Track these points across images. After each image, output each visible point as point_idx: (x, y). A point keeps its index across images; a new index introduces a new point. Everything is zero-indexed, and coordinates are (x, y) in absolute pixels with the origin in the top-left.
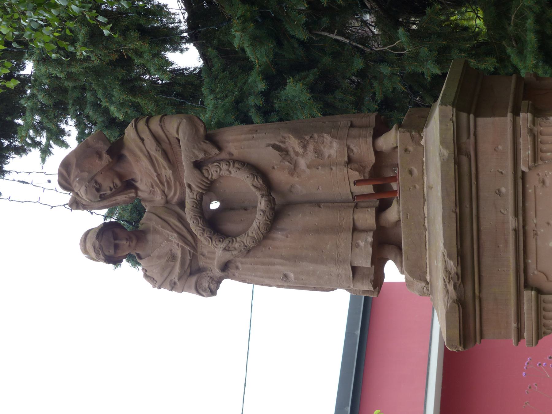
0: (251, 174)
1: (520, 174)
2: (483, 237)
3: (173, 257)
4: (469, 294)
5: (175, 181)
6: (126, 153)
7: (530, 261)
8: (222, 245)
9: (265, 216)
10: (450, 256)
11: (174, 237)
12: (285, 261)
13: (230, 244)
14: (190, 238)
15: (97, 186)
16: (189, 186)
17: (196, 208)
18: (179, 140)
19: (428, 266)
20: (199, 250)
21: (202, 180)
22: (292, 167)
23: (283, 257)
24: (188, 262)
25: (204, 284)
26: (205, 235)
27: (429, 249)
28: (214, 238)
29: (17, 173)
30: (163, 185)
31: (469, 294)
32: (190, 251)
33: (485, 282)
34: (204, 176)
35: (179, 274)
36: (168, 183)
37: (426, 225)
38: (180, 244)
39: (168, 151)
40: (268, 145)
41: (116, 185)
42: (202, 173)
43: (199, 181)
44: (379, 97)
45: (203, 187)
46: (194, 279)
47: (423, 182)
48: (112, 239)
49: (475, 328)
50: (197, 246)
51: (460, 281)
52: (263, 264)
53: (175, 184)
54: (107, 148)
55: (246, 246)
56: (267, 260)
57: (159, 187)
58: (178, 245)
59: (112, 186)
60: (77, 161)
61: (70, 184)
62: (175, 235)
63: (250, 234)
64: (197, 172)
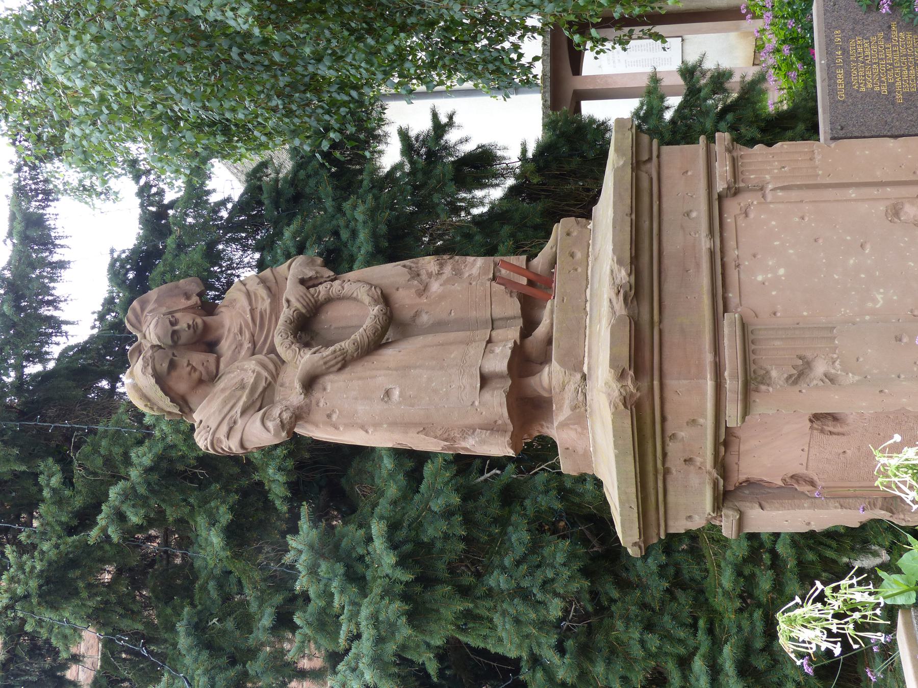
1: (716, 196)
2: (666, 262)
4: (645, 317)
7: (730, 295)
10: (620, 262)
16: (288, 301)
19: (586, 354)
20: (279, 380)
22: (421, 287)
24: (260, 389)
27: (590, 327)
31: (645, 317)
32: (266, 379)
33: (667, 312)
35: (245, 403)
37: (588, 309)
44: (530, 512)
47: (588, 265)
49: (653, 363)
51: (633, 292)
52: (359, 378)
57: (249, 328)
58: (253, 372)
61: (140, 322)
64: (302, 288)
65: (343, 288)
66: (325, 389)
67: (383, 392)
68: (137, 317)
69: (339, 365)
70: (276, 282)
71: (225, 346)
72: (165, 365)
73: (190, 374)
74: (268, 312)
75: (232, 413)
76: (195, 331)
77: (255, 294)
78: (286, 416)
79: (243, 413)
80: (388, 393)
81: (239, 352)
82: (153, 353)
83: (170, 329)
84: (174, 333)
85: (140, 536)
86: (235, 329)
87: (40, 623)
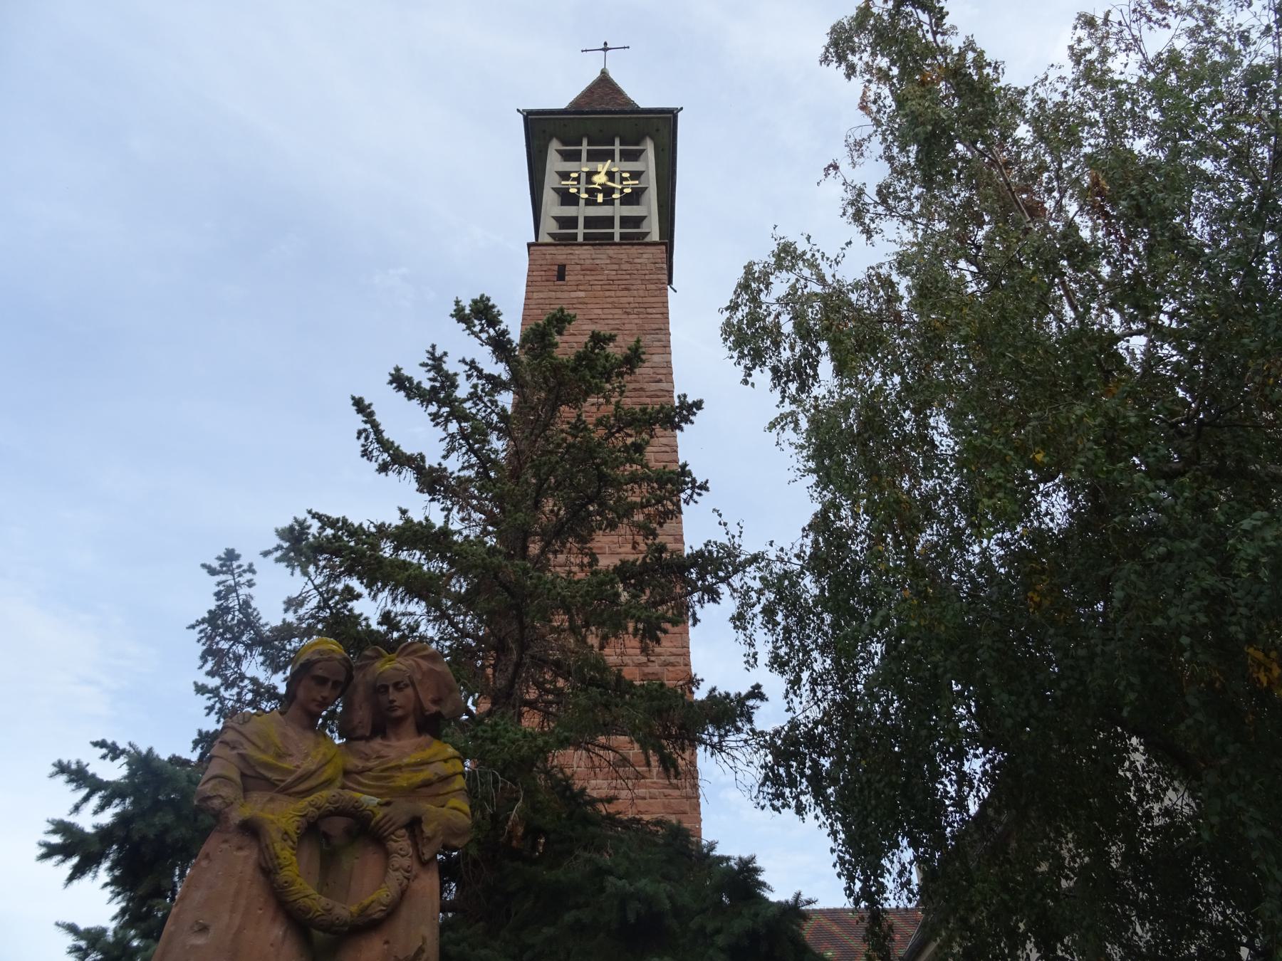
3: (280, 756)
5: (388, 788)
6: (426, 738)
8: (292, 829)
11: (309, 765)
14: (302, 787)
15: (402, 685)
16: (388, 804)
20: (280, 796)
28: (303, 820)
29: (778, 444)
30: (383, 771)
36: (385, 778)
39: (433, 787)
40: (424, 939)
42: (401, 828)
46: (235, 776)
53: (381, 787)
54: (444, 712)
57: (382, 763)
58: (298, 767)
61: (408, 655)
62: (313, 767)
63: (300, 880)
64: (404, 819)
65: (397, 870)
66: (240, 848)
68: (415, 652)
70: (439, 795)
71: (377, 744)
72: (320, 673)
73: (314, 700)
75: (247, 744)
78: (216, 803)
79: (242, 757)
80: (204, 929)
85: (1139, 758)
86: (384, 752)
87: (610, 175)
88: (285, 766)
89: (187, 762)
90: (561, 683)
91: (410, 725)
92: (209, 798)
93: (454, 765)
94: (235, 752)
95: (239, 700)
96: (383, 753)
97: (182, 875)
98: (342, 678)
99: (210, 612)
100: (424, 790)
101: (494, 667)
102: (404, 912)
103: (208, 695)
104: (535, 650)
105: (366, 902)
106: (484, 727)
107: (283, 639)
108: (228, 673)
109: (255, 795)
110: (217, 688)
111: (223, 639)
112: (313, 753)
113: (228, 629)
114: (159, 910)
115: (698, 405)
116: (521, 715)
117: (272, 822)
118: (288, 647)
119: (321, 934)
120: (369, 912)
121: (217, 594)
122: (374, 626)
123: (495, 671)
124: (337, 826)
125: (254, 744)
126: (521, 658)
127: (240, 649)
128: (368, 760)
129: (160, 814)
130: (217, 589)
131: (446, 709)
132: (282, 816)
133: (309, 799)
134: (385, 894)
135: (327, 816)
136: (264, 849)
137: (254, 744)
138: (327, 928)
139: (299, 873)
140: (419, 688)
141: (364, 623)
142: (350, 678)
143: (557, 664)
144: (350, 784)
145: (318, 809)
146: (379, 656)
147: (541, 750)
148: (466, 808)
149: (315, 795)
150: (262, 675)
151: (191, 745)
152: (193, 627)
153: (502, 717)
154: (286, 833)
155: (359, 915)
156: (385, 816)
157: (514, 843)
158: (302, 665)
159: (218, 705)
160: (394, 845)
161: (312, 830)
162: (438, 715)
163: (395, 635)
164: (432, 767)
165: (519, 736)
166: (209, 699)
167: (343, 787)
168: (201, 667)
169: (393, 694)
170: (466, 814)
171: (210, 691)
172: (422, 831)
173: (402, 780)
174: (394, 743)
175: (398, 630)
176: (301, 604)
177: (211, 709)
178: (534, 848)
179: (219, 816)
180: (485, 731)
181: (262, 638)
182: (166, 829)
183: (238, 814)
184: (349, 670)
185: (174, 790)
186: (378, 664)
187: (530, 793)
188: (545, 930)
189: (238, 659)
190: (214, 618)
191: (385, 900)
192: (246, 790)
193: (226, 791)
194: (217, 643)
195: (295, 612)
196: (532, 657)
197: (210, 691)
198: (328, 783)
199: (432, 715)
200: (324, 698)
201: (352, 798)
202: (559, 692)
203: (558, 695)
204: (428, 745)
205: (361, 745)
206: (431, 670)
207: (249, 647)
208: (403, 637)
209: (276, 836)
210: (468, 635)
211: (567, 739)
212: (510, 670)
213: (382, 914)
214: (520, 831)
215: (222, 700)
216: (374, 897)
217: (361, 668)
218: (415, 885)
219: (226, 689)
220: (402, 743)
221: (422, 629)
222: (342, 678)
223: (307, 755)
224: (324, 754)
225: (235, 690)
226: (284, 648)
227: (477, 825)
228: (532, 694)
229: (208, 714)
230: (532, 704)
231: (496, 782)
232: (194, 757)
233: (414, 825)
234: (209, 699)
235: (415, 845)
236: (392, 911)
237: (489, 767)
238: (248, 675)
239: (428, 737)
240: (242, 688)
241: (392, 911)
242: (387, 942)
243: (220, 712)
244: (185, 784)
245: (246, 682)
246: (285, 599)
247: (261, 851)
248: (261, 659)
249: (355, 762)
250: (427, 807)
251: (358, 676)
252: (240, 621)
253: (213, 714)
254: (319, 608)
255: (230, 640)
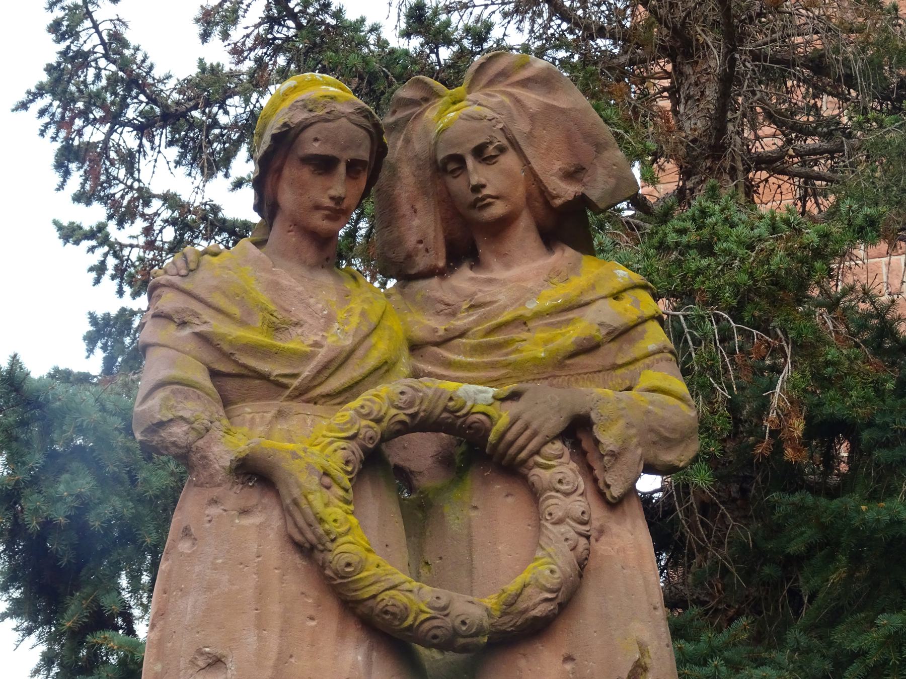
0: (561, 584)
3: (276, 329)
5: (507, 365)
6: (565, 255)
8: (335, 465)
9: (433, 613)
11: (338, 338)
12: (271, 663)
13: (341, 493)
15: (491, 151)
16: (515, 396)
17: (446, 409)
18: (629, 389)
20: (296, 406)
21: (535, 434)
23: (283, 658)
24: (264, 367)
25: (190, 405)
26: (364, 422)
28: (353, 445)
32: (295, 376)
34: (545, 443)
35: (223, 337)
36: (498, 346)
38: (322, 351)
40: (643, 648)
41: (490, 204)
43: (534, 425)
45: (509, 436)
48: (351, 154)
50: (308, 401)
52: (261, 592)
53: (493, 366)
54: (594, 194)
55: (333, 541)
56: (275, 608)
57: (477, 323)
58: (316, 344)
59: (486, 192)
60: (562, 111)
61: (491, 83)
62: (348, 342)
63: (373, 558)
64: (555, 422)
66: (245, 512)
67: (219, 651)
68: (504, 74)
69: (298, 537)
70: (615, 367)
71: (464, 279)
72: (315, 148)
73: (318, 207)
74: (513, 357)
75: (206, 314)
76: (473, 205)
77: (569, 322)
78: (178, 432)
79: (204, 338)
81: (438, 313)
82: (342, 115)
83: (465, 150)
84: (459, 160)
88: (291, 345)
89: (84, 378)
90: (828, 106)
91: (524, 232)
92: (161, 424)
93: (636, 303)
94: (187, 331)
95: (150, 245)
96: (480, 297)
97: (136, 587)
98: (364, 154)
99: (50, 69)
100: (582, 360)
101: (673, 93)
102: (591, 600)
103: (86, 244)
104: (759, 38)
105: (512, 587)
106: (679, 224)
107: (208, 103)
108: (117, 190)
109: (246, 410)
110: (101, 227)
111: (87, 122)
112: (341, 315)
113: (94, 100)
114: (110, 651)
115: (88, 252)
116: (750, 190)
117: (295, 455)
118: (223, 119)
119: (435, 654)
120: (521, 605)
121: (55, 27)
122: (396, 42)
123: (676, 103)
124: (420, 452)
125: (219, 310)
126: (732, 62)
127: (128, 139)
128: (453, 314)
129: (65, 477)
130: (50, 18)
131: (597, 189)
132: (312, 443)
133: (356, 403)
134: (547, 568)
135: (399, 433)
136: (290, 509)
137: (219, 310)
138: (446, 643)
139: (368, 540)
140: (529, 152)
141: (372, 39)
142: (380, 150)
143: (818, 65)
144: (429, 368)
145: (378, 421)
146: (430, 96)
147: (818, 253)
148: (679, 385)
149: (365, 395)
150: (185, 184)
151: (84, 346)
152: (24, 106)
153: (713, 194)
154: (326, 474)
155: (504, 614)
156: (513, 423)
157: (789, 453)
158: (274, 137)
159: (111, 262)
160: (545, 474)
161: (374, 463)
162: (582, 203)
163: (445, 53)
164: (590, 313)
165: (762, 229)
166: (92, 249)
167: (416, 374)
168: (61, 187)
169: (477, 173)
170: (681, 399)
171: (90, 235)
172: (597, 442)
173: (536, 345)
174: (499, 272)
175: (448, 42)
176: (232, 18)
177: (100, 269)
178: (830, 459)
179: (187, 459)
180: (682, 232)
181: (164, 107)
182: (84, 506)
183: (226, 447)
184: (376, 134)
185: (80, 430)
186: (430, 114)
187: (806, 349)
188: (882, 620)
189: (129, 160)
190: (60, 80)
191: (553, 581)
192: (226, 402)
193: (190, 408)
194: (80, 133)
195: (225, 36)
196: (756, 56)
197: (90, 235)
198: (383, 370)
199: (568, 204)
200: (338, 200)
201: (439, 394)
202: (830, 129)
203: (828, 136)
204: (574, 269)
205: (432, 287)
206: (550, 109)
207: (144, 129)
208: (463, 55)
209: (311, 482)
210: (601, 32)
211: (872, 222)
212: (712, 92)
213: (549, 607)
214: (798, 426)
215: (116, 249)
216: (525, 576)
217: (395, 127)
218: (602, 547)
219: (120, 224)
220: (515, 272)
221: (496, 33)
222: (364, 154)
223: (330, 319)
224: (363, 314)
225: (140, 224)
226: (215, 124)
227: (704, 428)
228: (769, 140)
229: (97, 281)
230: (772, 163)
231: (726, 337)
232: (94, 365)
233: (577, 431)
234: (92, 249)
235: (588, 470)
236: (566, 601)
237: (706, 304)
238: (156, 189)
239: (569, 252)
240: (151, 219)
241: (566, 601)
242: (568, 659)
243: (120, 272)
244: (96, 416)
245: (156, 204)
246: (198, 13)
247: (286, 512)
248: (174, 152)
249: (428, 324)
250: (598, 395)
251: (395, 146)
252: (113, 80)
253: (106, 278)
254: (271, 21)
255: (102, 121)
